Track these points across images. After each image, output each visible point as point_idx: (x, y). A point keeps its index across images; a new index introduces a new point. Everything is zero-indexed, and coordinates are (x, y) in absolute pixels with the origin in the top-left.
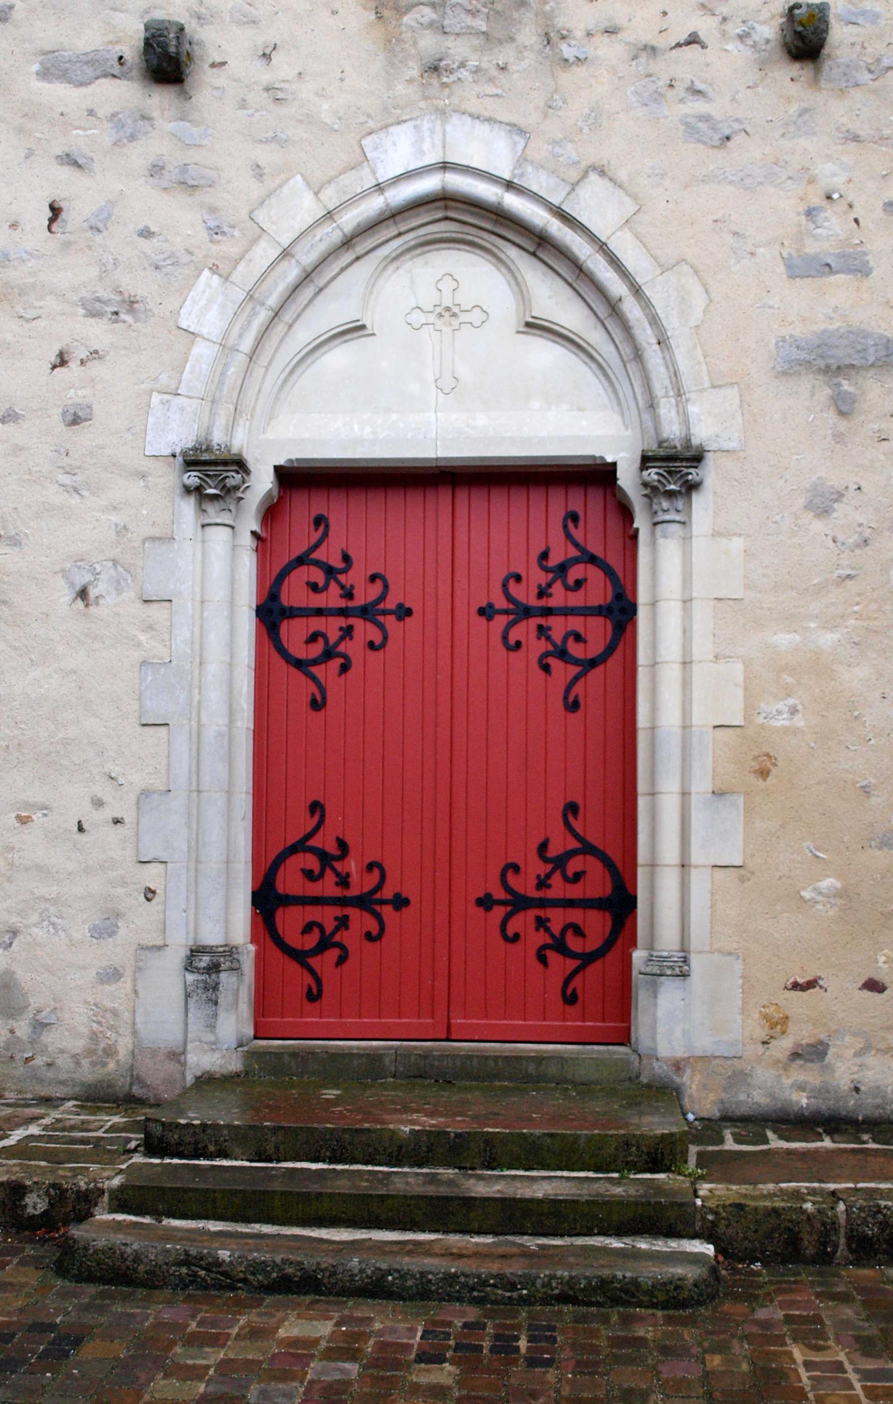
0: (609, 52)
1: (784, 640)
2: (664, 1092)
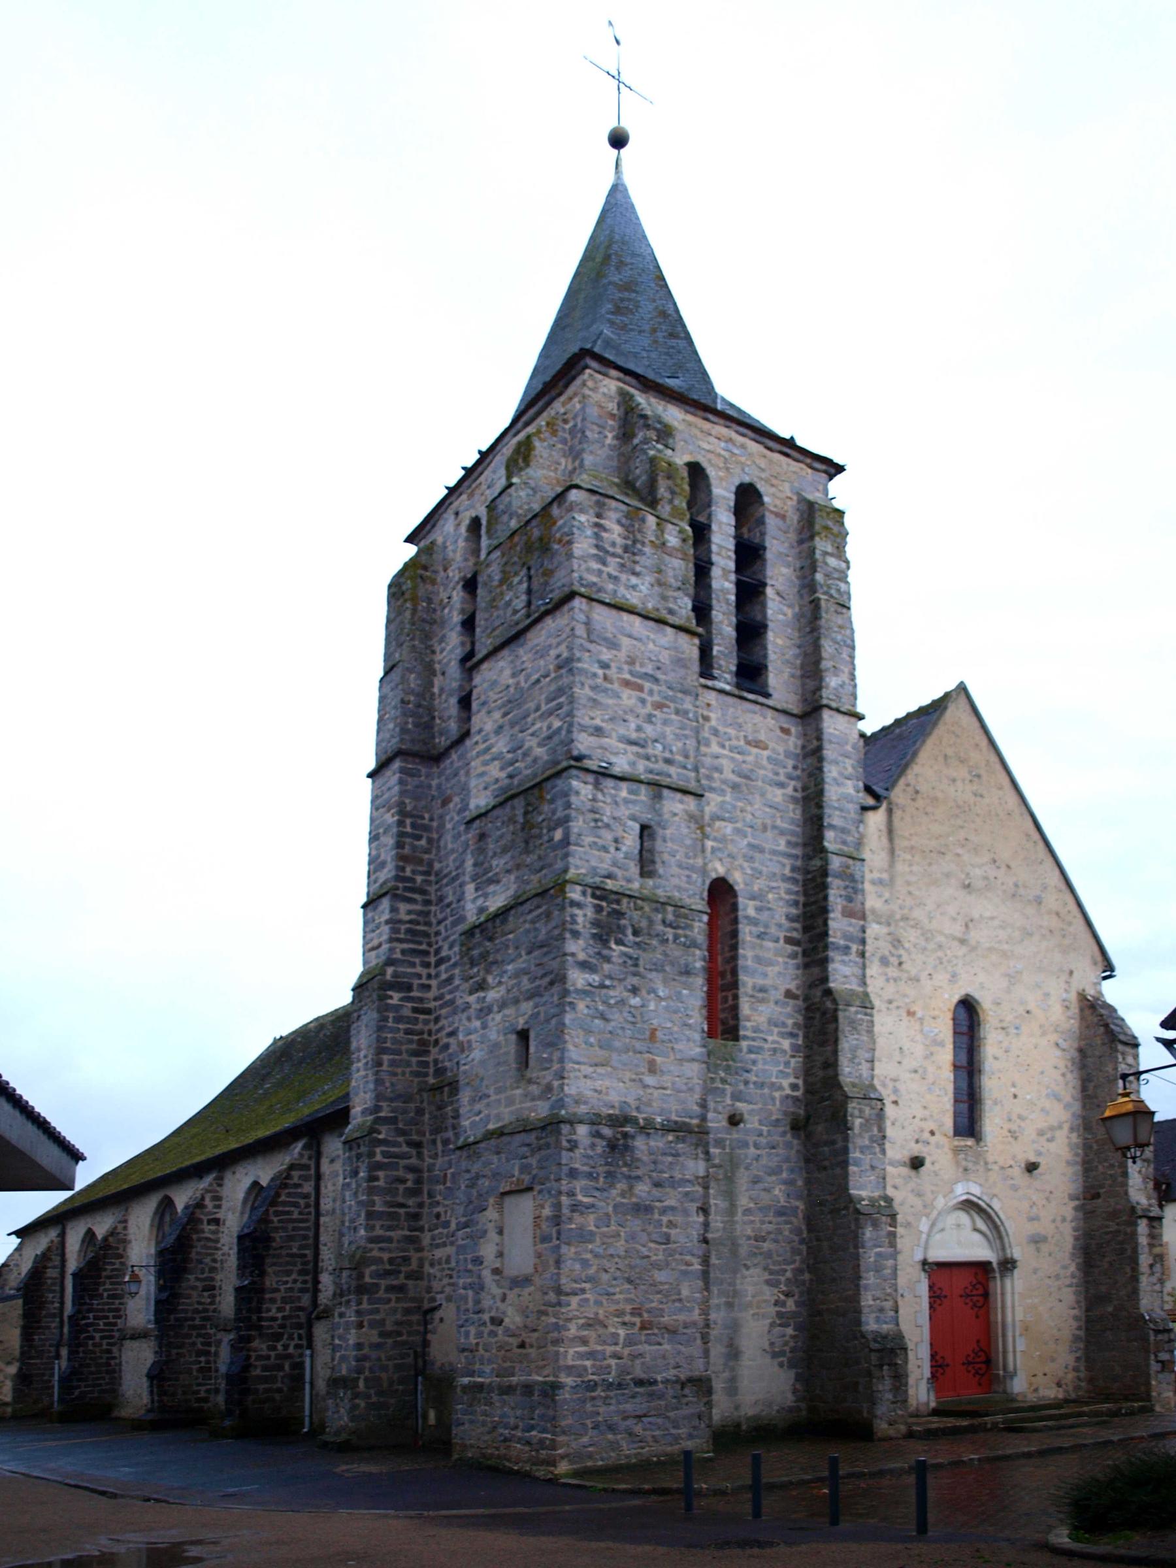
0: (996, 1168)
1: (1029, 1301)
2: (1013, 1400)
